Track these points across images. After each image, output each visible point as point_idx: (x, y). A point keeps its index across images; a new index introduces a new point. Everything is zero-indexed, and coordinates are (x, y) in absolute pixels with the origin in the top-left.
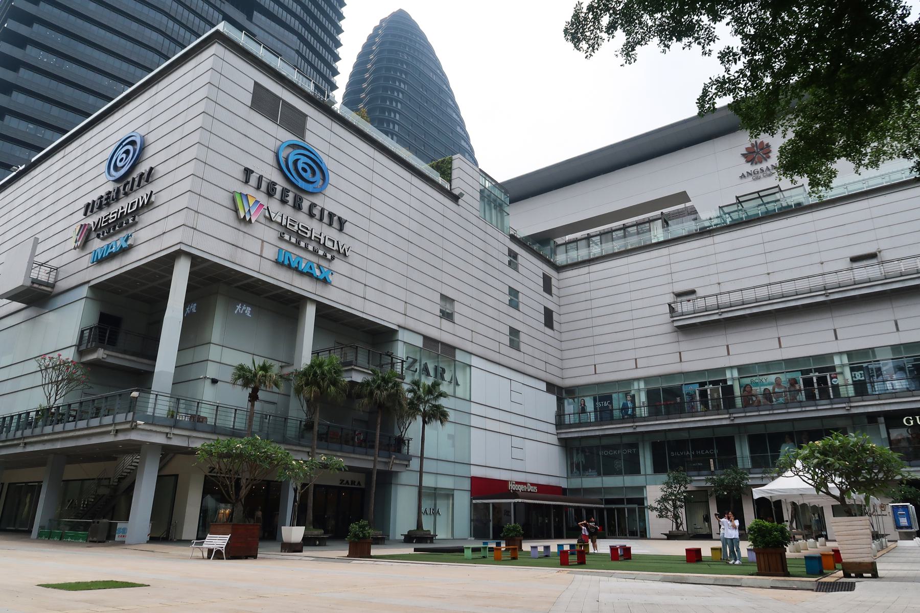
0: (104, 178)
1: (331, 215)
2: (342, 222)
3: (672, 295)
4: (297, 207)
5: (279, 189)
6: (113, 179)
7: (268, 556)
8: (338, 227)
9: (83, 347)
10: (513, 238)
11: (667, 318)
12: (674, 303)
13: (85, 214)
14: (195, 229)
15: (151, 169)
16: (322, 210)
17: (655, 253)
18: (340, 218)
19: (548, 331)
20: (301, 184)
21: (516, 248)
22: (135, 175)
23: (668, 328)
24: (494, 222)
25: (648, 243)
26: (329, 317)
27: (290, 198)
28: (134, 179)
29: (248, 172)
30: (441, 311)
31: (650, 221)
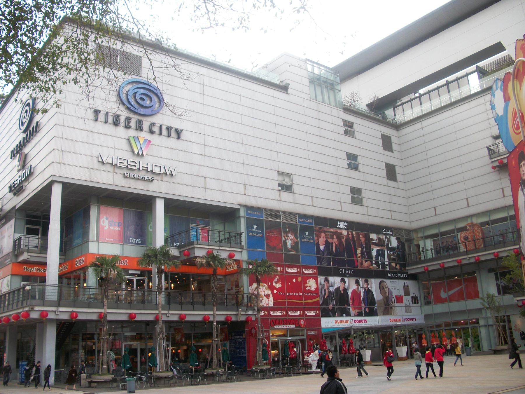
0: (19, 132)
1: (169, 129)
2: (178, 133)
3: (491, 139)
4: (139, 127)
5: (122, 119)
6: (22, 131)
7: (106, 387)
8: (176, 136)
9: (16, 253)
10: (347, 110)
11: (487, 160)
12: (493, 145)
13: (11, 158)
14: (61, 163)
15: (37, 122)
16: (161, 127)
17: (473, 103)
18: (176, 130)
19: (391, 183)
20: (142, 111)
21: (350, 118)
22: (31, 128)
23: (489, 168)
24: (326, 100)
25: (469, 94)
26: (174, 207)
27: (133, 124)
28: (30, 131)
29: (97, 112)
30: (280, 185)
31: (467, 75)
